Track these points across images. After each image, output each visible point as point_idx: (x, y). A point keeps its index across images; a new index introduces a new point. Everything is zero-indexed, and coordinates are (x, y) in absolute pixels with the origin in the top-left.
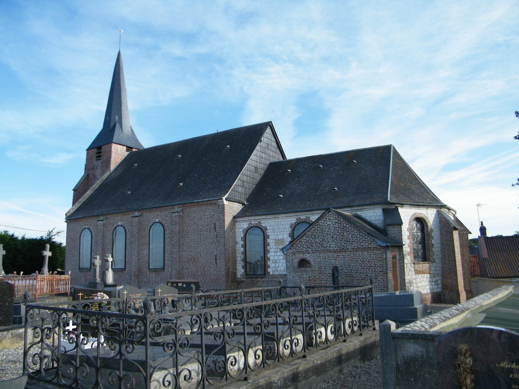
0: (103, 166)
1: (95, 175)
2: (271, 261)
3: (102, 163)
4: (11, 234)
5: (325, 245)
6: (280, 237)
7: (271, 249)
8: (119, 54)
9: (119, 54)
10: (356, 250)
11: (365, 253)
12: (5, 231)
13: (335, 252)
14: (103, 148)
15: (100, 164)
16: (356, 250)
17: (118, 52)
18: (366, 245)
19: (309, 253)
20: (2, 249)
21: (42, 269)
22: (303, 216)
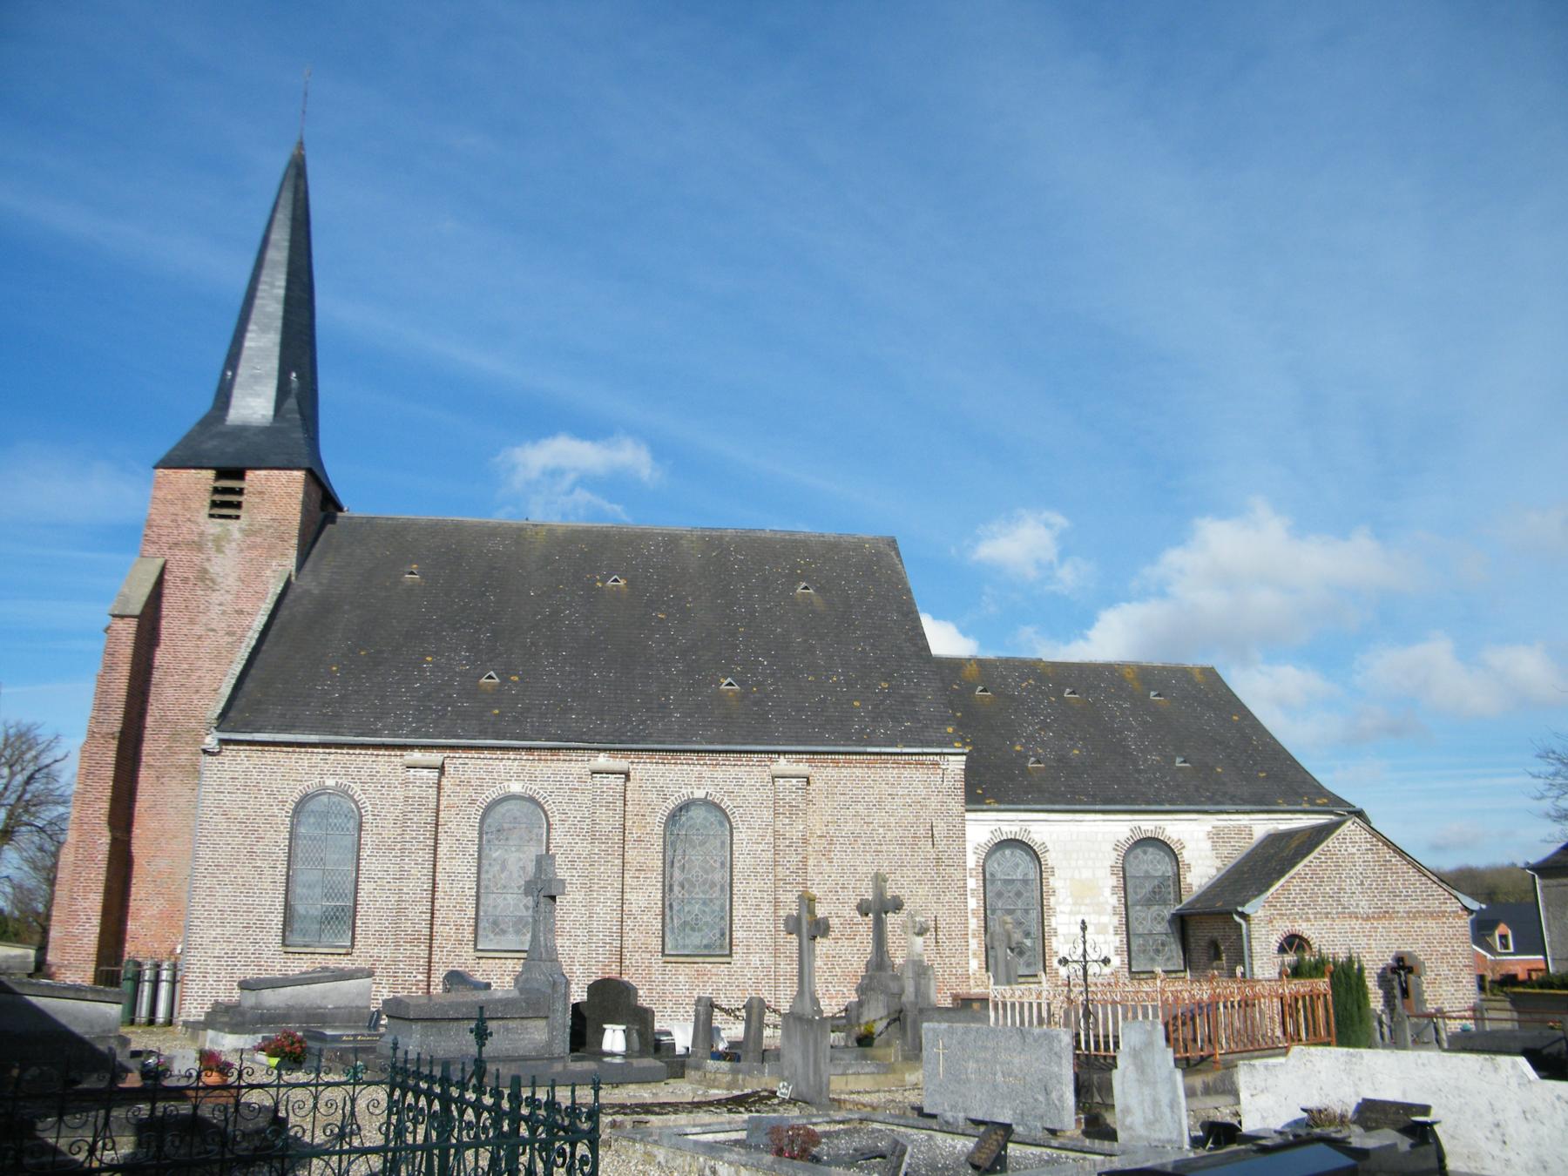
0: (252, 547)
1: (205, 571)
2: (1061, 938)
3: (248, 533)
4: (1342, 957)
5: (1344, 901)
6: (1086, 874)
7: (1058, 903)
8: (298, 172)
9: (298, 172)
10: (1413, 915)
11: (1431, 923)
12: (527, 893)
13: (1368, 918)
14: (250, 475)
15: (237, 535)
16: (1413, 915)
17: (279, 163)
18: (1435, 905)
19: (1308, 920)
20: (1314, 1103)
21: (1169, 1169)
22: (1148, 824)
